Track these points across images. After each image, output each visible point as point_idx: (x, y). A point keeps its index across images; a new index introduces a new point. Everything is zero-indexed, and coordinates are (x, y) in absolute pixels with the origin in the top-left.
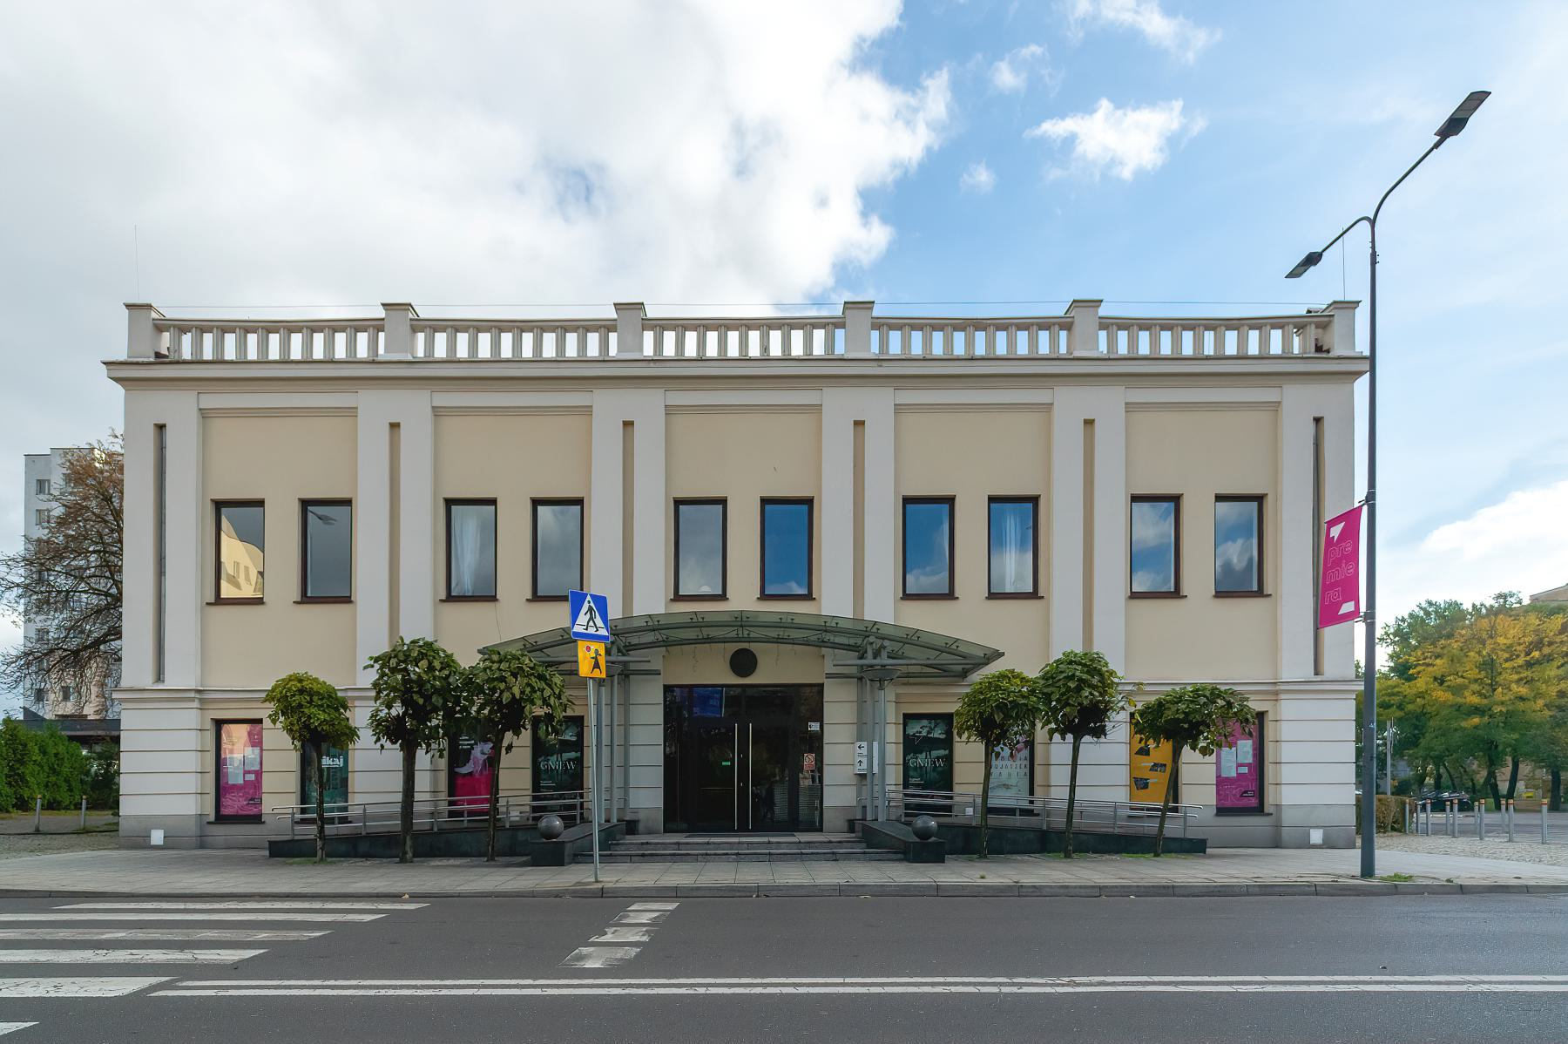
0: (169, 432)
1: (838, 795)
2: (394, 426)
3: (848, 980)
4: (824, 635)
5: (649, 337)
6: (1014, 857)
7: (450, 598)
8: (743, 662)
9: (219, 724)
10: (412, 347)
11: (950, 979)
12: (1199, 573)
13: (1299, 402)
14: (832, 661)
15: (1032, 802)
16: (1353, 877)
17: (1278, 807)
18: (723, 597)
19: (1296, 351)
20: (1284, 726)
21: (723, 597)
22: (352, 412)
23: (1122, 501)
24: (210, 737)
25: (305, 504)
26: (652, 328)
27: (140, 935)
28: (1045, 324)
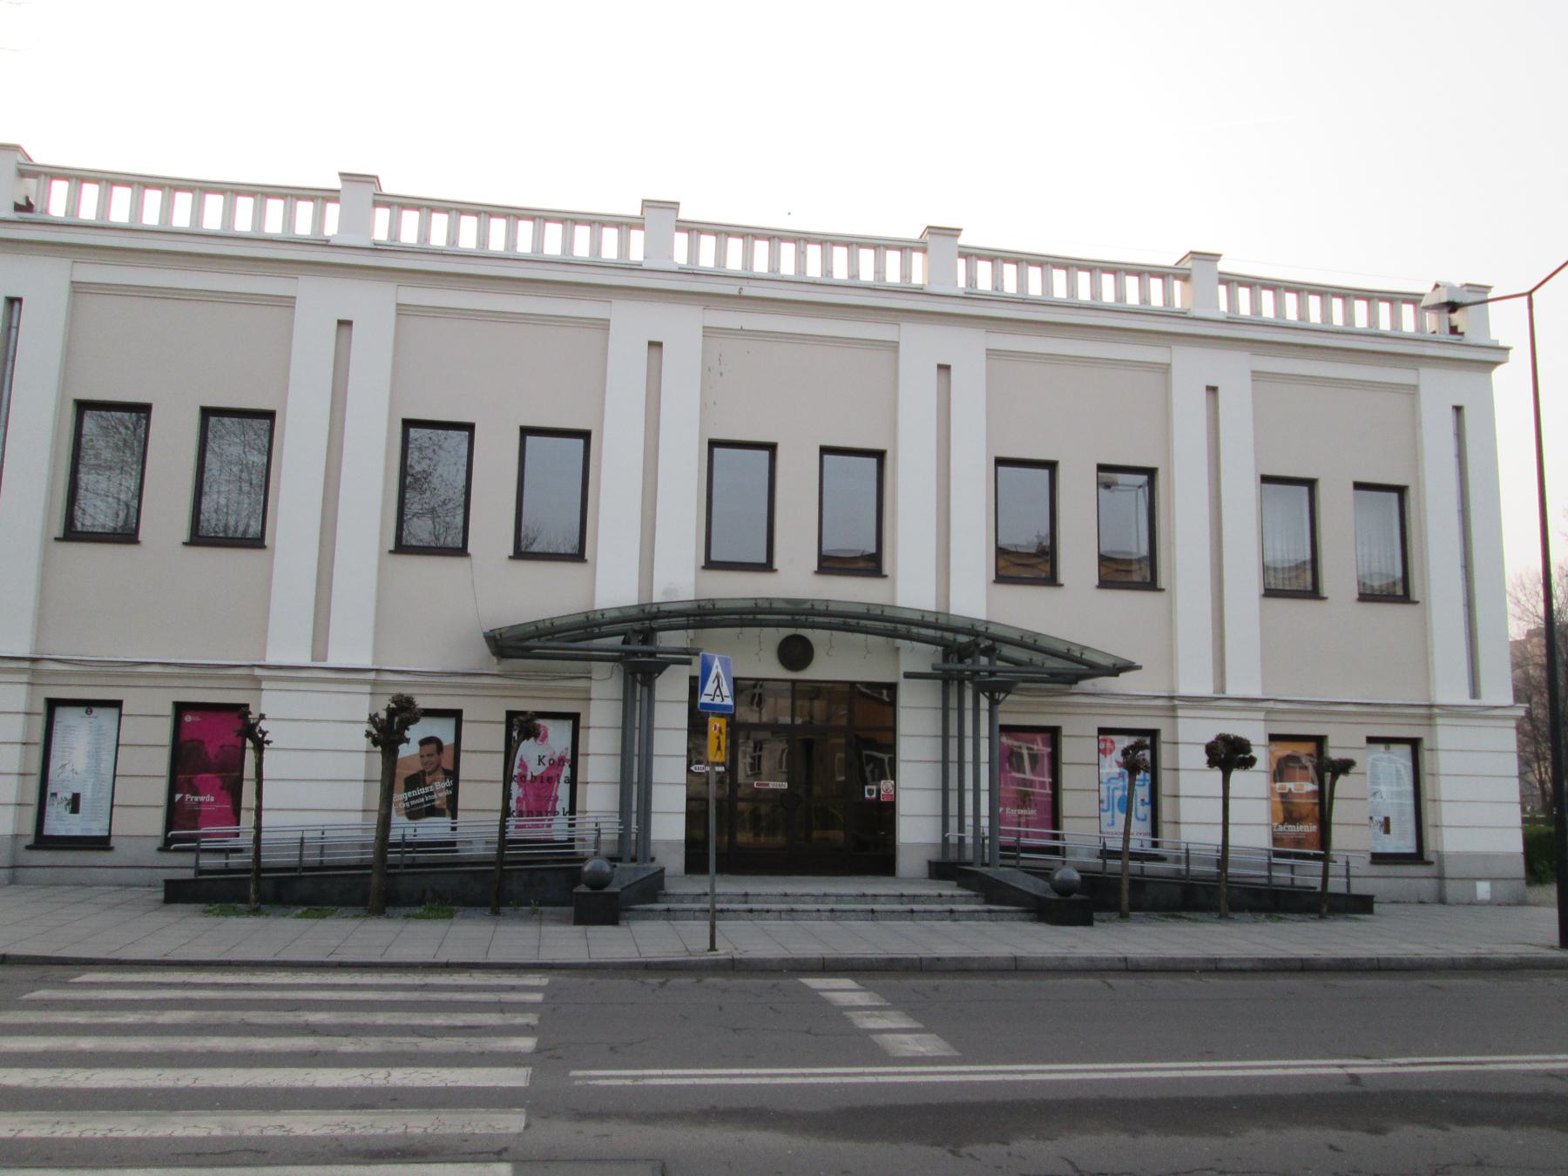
0: (1467, 412)
1: (916, 828)
2: (944, 368)
3: (666, 1072)
4: (892, 626)
5: (382, 215)
6: (1289, 916)
7: (71, 533)
8: (795, 653)
9: (53, 704)
10: (369, 225)
11: (1480, 1067)
12: (1339, 578)
13: (1438, 390)
14: (918, 657)
15: (454, 829)
16: (1552, 947)
17: (1440, 855)
18: (768, 566)
19: (1178, 304)
20: (1442, 756)
21: (768, 566)
22: (288, 302)
23: (1251, 485)
24: (39, 723)
25: (207, 413)
26: (389, 205)
27: (216, 1016)
28: (1163, 274)
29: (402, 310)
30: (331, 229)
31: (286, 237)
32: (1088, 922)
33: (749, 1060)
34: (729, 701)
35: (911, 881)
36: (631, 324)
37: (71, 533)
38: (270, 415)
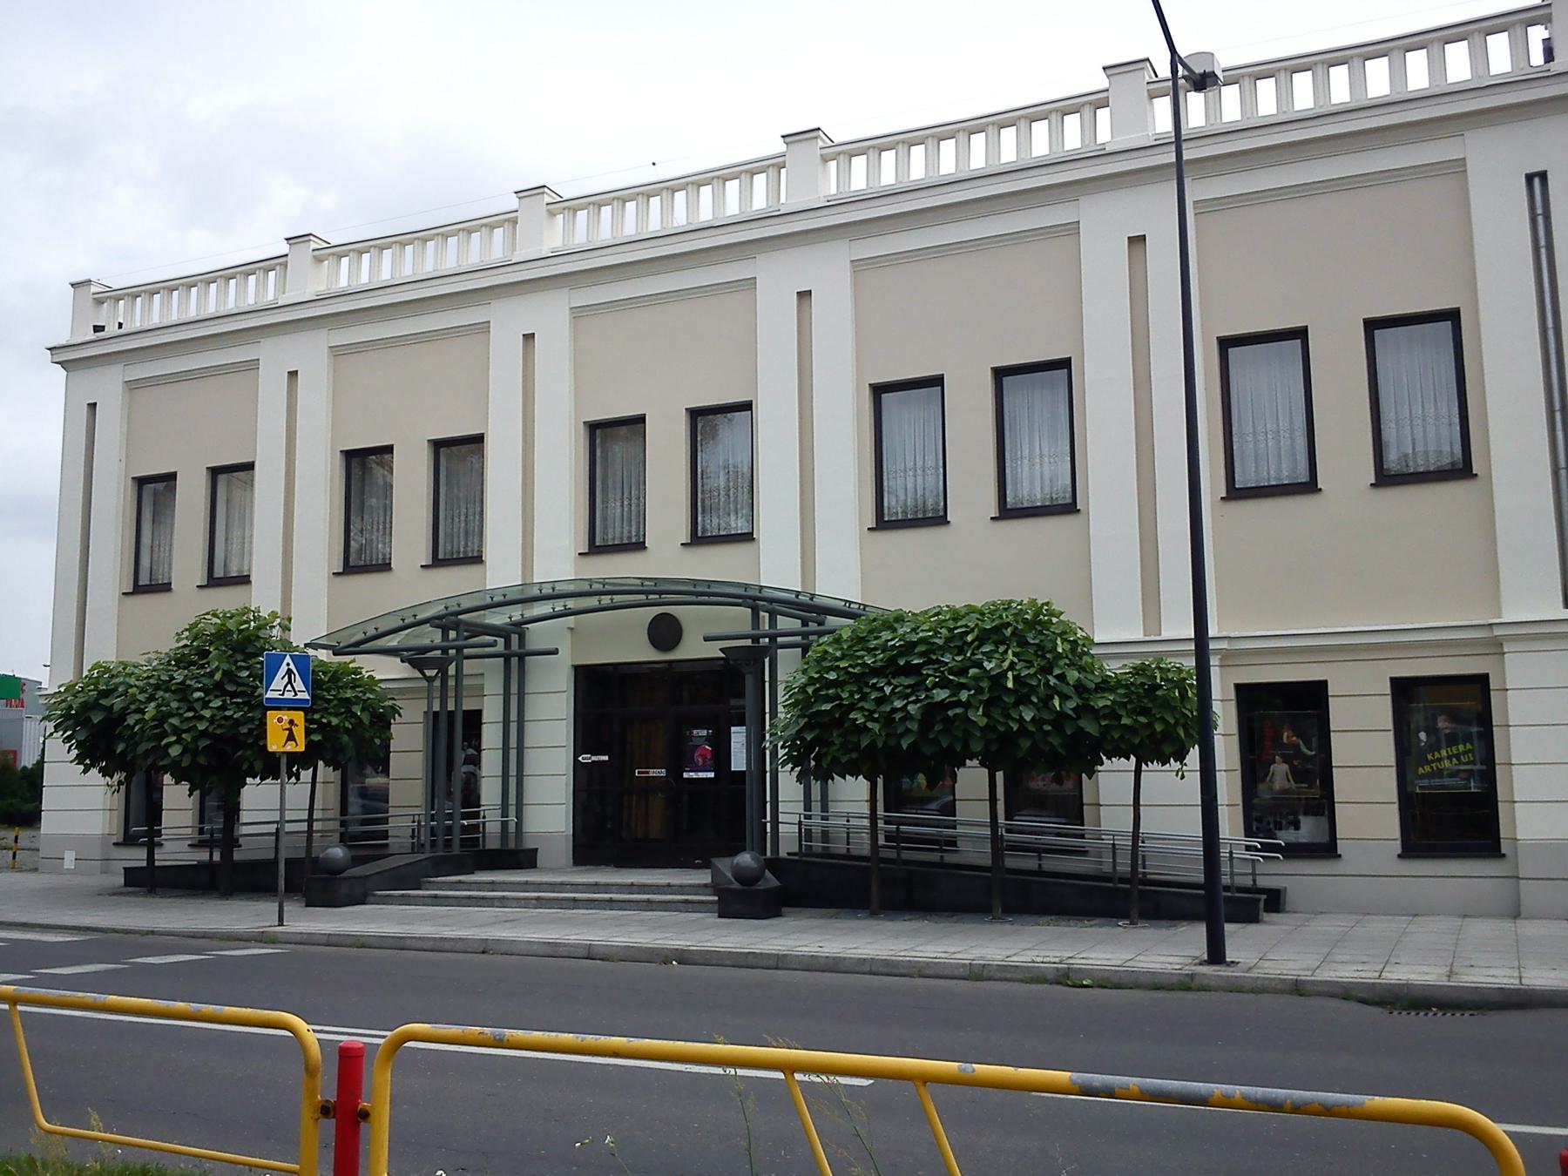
4: (755, 600)
10: (1146, 117)
22: (253, 365)
29: (337, 352)
30: (1104, 135)
31: (1054, 158)
32: (779, 915)
33: (1550, 1136)
34: (306, 696)
35: (552, 870)
36: (777, 280)
37: (883, 523)
38: (1065, 364)
